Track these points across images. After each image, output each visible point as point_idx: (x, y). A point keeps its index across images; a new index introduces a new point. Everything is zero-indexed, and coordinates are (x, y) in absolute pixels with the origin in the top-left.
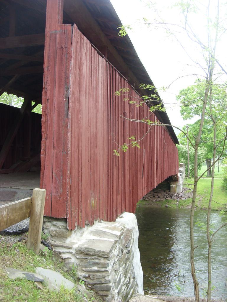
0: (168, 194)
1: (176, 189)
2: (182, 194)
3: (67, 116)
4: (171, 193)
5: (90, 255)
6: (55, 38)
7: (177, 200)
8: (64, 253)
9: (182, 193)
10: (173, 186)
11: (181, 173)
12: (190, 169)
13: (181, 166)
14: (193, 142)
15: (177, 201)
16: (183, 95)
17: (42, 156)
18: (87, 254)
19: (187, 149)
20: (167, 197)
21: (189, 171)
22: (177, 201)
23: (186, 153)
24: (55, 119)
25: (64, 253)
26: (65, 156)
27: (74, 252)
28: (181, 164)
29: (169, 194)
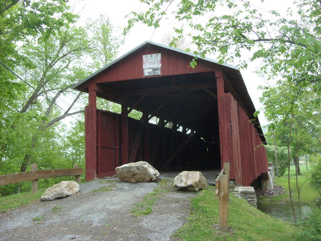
0: (260, 192)
1: (267, 187)
2: (273, 191)
3: (232, 134)
4: (263, 190)
5: (247, 194)
6: (223, 99)
7: (269, 196)
8: (235, 194)
9: (273, 190)
10: (264, 184)
11: (271, 172)
12: (278, 168)
13: (270, 165)
14: (279, 141)
15: (269, 198)
16: (266, 97)
17: (221, 152)
18: (245, 194)
19: (274, 149)
20: (259, 195)
21: (278, 170)
22: (269, 198)
23: (273, 152)
24: (226, 136)
25: (235, 194)
26: (233, 152)
27: (239, 193)
28: (269, 164)
29: (261, 192)
